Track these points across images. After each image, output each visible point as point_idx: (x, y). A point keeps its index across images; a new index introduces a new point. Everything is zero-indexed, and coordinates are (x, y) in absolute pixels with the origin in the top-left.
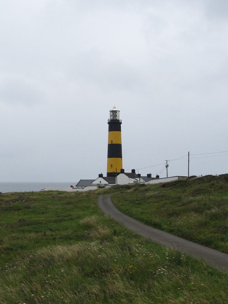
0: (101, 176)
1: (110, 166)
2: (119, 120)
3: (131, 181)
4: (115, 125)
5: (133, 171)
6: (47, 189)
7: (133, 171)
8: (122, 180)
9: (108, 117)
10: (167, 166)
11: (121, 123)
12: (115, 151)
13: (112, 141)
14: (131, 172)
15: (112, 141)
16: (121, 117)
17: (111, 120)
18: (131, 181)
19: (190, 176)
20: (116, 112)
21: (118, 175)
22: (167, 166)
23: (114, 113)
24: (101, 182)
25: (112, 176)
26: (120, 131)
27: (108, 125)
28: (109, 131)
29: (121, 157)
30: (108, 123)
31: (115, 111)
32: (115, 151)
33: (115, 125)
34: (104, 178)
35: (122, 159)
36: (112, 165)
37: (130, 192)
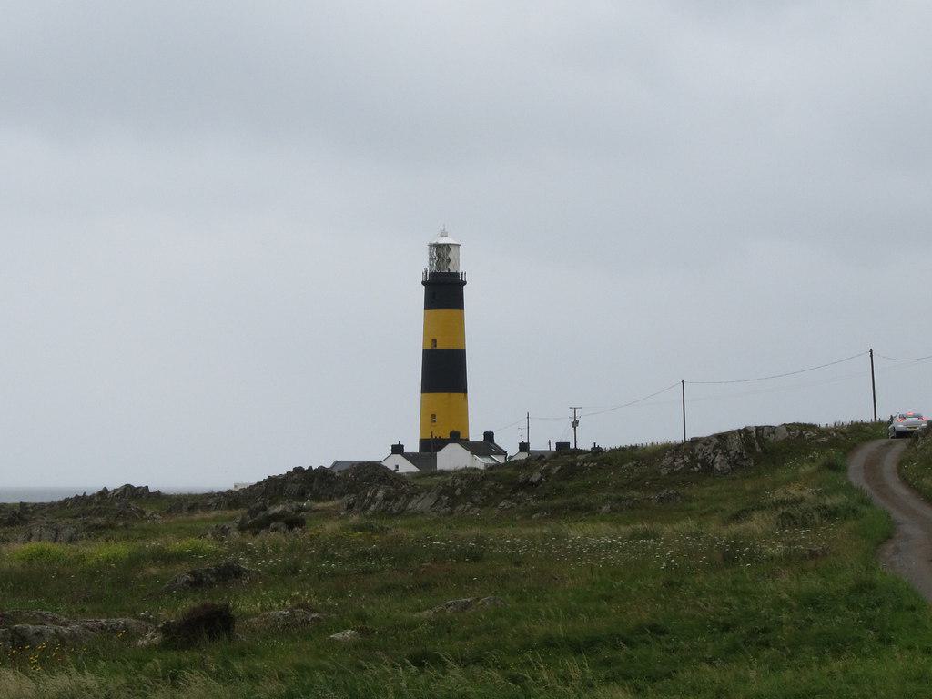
0: (397, 449)
1: (430, 417)
2: (457, 274)
3: (481, 463)
4: (444, 290)
5: (489, 436)
6: (194, 493)
7: (489, 436)
8: (452, 458)
9: (421, 264)
10: (575, 424)
11: (465, 283)
12: (444, 371)
13: (434, 341)
14: (481, 438)
15: (434, 341)
16: (465, 265)
17: (433, 275)
18: (481, 463)
19: (688, 438)
20: (449, 249)
21: (439, 448)
22: (575, 424)
23: (441, 252)
24: (397, 467)
25: (431, 446)
26: (462, 308)
27: (423, 288)
28: (427, 308)
29: (465, 391)
30: (424, 283)
31: (444, 245)
32: (444, 371)
33: (444, 290)
34: (411, 457)
35: (466, 396)
36: (433, 416)
37: (331, 498)
